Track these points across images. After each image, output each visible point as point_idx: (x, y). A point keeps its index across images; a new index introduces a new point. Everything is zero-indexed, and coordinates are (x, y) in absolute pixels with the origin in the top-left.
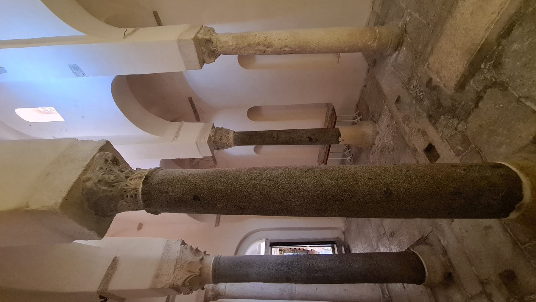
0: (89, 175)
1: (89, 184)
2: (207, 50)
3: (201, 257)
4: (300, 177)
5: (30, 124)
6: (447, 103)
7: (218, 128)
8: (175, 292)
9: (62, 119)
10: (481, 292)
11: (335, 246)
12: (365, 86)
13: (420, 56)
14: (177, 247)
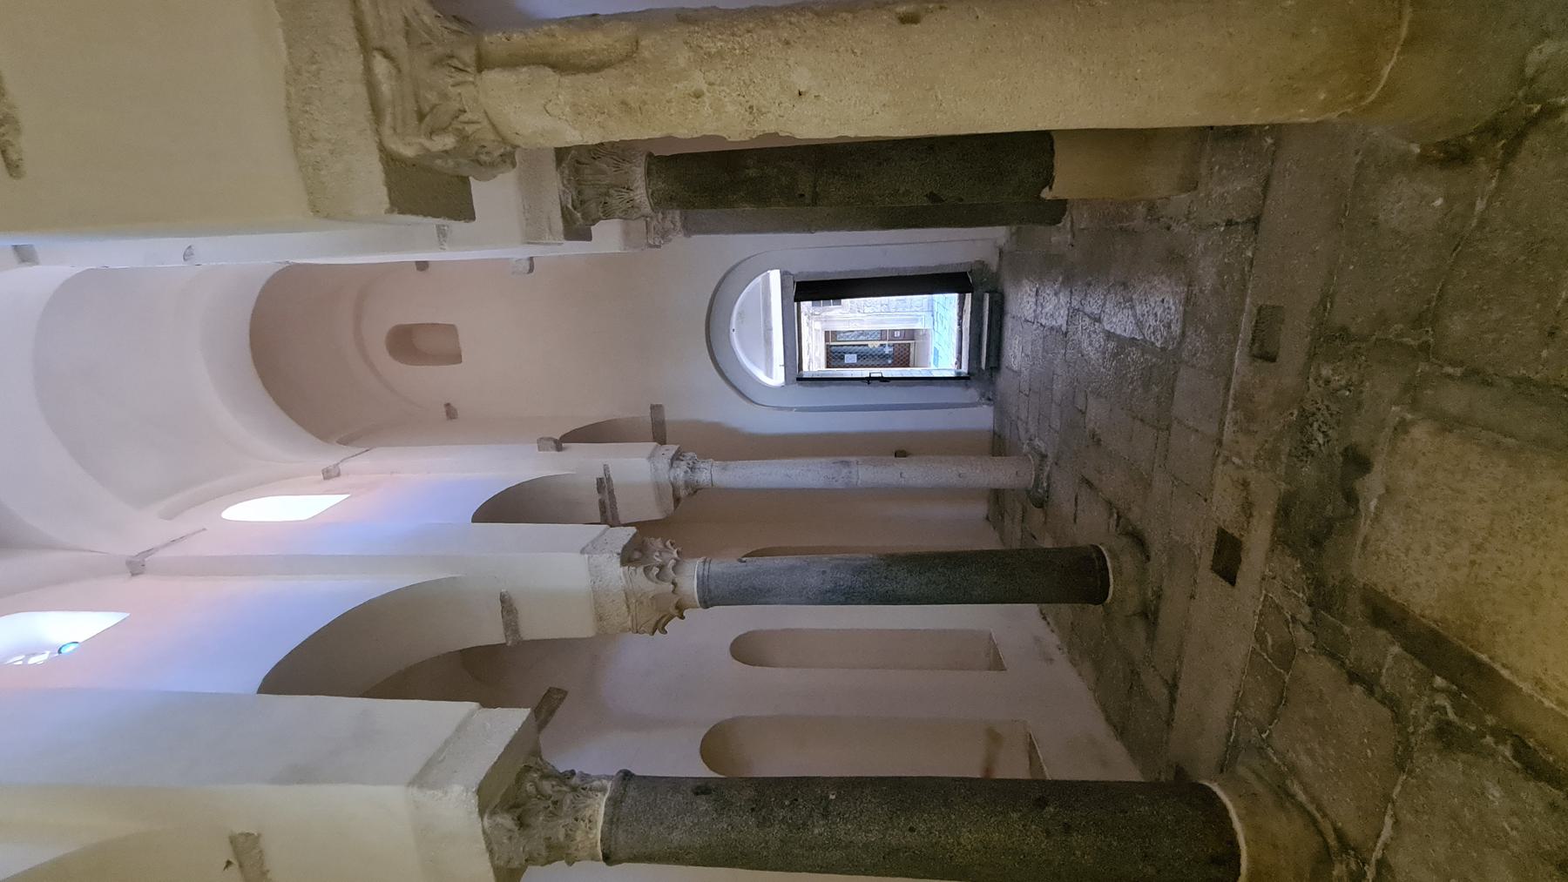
11: (969, 296)
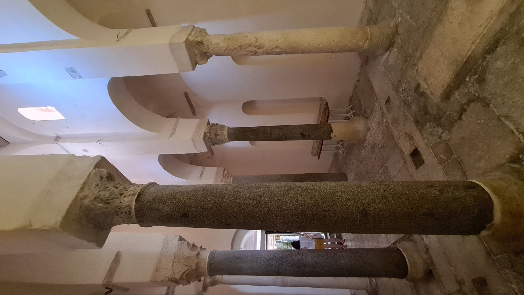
0: (86, 192)
1: (86, 202)
2: (198, 51)
3: (197, 252)
4: (282, 196)
5: (33, 122)
6: (433, 111)
7: (213, 124)
8: (174, 284)
9: (63, 118)
10: (458, 291)
12: (358, 81)
13: (409, 61)
14: (175, 242)
